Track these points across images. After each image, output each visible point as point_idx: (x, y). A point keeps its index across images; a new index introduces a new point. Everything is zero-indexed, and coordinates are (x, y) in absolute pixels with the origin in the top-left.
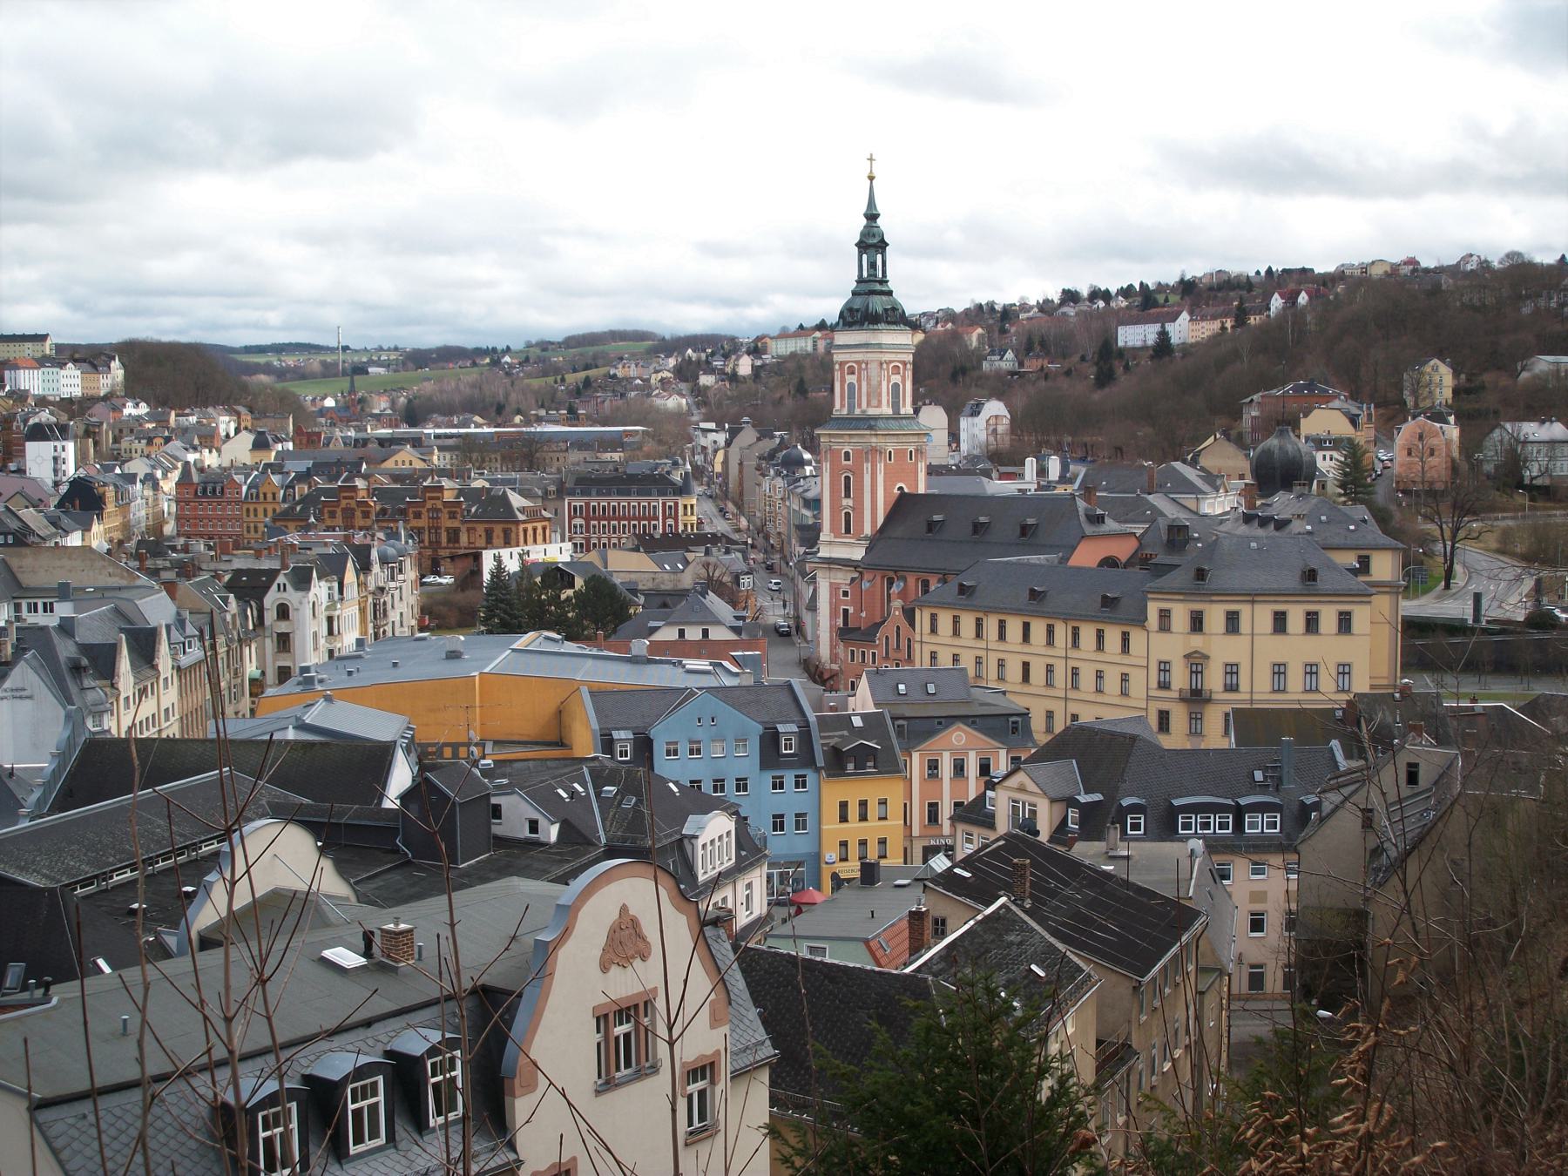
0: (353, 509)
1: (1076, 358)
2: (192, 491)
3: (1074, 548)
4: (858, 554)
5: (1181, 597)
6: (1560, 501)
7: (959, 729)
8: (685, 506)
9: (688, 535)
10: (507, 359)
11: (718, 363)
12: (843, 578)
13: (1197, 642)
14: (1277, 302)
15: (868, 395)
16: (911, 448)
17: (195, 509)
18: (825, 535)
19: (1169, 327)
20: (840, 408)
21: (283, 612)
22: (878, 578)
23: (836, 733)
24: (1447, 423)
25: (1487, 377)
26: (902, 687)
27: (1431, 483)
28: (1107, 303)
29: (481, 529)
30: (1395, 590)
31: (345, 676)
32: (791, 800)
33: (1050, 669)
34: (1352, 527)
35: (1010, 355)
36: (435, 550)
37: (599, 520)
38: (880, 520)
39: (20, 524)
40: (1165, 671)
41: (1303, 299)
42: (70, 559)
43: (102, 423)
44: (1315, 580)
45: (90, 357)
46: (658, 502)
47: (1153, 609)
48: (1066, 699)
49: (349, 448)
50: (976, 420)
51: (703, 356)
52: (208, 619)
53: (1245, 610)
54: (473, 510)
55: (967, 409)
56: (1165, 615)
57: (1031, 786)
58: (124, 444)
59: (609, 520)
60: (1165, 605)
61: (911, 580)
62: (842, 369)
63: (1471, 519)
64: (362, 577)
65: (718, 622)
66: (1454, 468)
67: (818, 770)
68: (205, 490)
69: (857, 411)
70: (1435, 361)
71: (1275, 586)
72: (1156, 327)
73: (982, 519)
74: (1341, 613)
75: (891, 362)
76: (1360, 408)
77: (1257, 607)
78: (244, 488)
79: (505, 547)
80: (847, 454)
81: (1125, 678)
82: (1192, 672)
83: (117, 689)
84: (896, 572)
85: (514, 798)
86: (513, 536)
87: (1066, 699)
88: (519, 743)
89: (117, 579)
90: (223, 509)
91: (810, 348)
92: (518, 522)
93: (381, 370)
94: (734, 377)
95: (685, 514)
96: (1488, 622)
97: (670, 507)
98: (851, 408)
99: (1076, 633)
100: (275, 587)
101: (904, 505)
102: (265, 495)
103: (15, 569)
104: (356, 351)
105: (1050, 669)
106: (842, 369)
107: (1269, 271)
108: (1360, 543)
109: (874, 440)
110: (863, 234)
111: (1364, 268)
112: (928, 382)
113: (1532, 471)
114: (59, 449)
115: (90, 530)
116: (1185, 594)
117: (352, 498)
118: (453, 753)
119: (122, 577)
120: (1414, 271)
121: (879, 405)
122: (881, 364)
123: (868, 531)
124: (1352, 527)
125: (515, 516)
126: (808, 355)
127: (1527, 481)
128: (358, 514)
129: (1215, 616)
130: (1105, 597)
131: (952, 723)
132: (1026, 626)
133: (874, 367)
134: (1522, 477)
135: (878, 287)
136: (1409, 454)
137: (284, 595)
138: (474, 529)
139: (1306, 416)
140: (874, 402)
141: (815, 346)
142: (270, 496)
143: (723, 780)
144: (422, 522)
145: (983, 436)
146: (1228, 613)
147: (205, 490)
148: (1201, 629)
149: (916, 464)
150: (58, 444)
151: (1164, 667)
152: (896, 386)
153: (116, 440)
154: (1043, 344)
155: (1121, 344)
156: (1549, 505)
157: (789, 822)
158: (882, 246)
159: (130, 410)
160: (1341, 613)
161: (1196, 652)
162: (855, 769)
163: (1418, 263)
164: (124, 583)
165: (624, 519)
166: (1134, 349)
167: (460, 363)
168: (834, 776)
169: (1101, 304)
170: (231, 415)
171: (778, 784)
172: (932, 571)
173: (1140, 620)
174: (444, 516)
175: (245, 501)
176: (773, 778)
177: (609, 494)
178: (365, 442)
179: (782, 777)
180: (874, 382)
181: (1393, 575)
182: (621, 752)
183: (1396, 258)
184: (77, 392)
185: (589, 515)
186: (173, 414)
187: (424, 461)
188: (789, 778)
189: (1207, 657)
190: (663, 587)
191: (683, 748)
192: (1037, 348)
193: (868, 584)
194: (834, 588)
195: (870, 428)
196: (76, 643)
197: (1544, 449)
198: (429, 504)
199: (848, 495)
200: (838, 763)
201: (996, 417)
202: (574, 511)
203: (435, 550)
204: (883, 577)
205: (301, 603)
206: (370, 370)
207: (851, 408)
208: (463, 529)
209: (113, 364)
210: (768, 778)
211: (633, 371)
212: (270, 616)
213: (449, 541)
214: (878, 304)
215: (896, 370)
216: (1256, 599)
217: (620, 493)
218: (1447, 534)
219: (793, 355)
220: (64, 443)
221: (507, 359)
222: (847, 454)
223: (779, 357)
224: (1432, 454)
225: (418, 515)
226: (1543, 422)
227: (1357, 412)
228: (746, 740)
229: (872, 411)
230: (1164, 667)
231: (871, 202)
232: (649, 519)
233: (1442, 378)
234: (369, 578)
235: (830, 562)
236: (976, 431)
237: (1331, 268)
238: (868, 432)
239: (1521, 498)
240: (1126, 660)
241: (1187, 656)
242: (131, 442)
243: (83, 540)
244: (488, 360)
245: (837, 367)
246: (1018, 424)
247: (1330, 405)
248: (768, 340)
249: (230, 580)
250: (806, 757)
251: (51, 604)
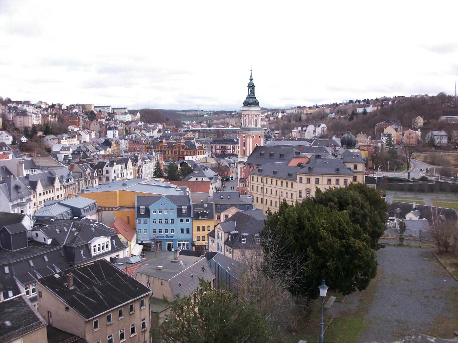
0: (180, 147)
2: (133, 142)
3: (291, 161)
4: (245, 160)
5: (305, 174)
6: (442, 149)
7: (233, 208)
8: (237, 147)
9: (227, 154)
10: (233, 113)
11: (274, 115)
12: (242, 166)
13: (308, 186)
15: (249, 122)
16: (260, 135)
17: (133, 146)
19: (366, 108)
21: (107, 172)
22: (248, 166)
23: (199, 208)
24: (418, 131)
25: (431, 121)
26: (222, 196)
27: (412, 145)
28: (359, 103)
29: (189, 151)
30: (363, 174)
31: (96, 189)
32: (185, 225)
33: (276, 191)
34: (353, 157)
36: (179, 156)
37: (218, 150)
38: (251, 152)
39: (86, 149)
40: (301, 193)
42: (46, 160)
43: (131, 127)
44: (338, 171)
45: (133, 112)
47: (298, 177)
48: (280, 199)
49: (184, 132)
50: (319, 128)
51: (272, 113)
52: (80, 174)
53: (320, 178)
54: (187, 147)
55: (317, 126)
56: (301, 179)
58: (136, 131)
59: (220, 150)
60: (301, 176)
61: (255, 167)
62: (243, 116)
63: (414, 153)
64: (134, 163)
65: (205, 177)
66: (418, 142)
67: (192, 218)
68: (135, 142)
69: (246, 126)
70: (419, 117)
71: (328, 172)
72: (363, 108)
73: (272, 153)
74: (345, 180)
75: (255, 114)
76: (398, 127)
77: (323, 177)
78: (143, 141)
79: (190, 156)
81: (292, 194)
82: (307, 193)
83: (36, 192)
84: (251, 165)
85: (40, 232)
86: (196, 153)
87: (280, 199)
88: (128, 207)
89: (56, 164)
91: (294, 112)
92: (197, 150)
93: (207, 116)
94: (277, 118)
95: (237, 149)
96: (411, 179)
97: (234, 147)
100: (105, 166)
101: (257, 149)
102: (148, 143)
103: (35, 162)
104: (205, 111)
105: (276, 191)
106: (243, 116)
107: (395, 97)
108: (355, 161)
109: (249, 133)
110: (249, 84)
111: (416, 96)
112: (316, 120)
113: (436, 142)
114: (115, 132)
115: (106, 150)
116: (306, 174)
117: (162, 144)
118: (112, 209)
119: (57, 164)
121: (251, 124)
122: (252, 115)
123: (248, 155)
124: (353, 157)
125: (196, 148)
126: (294, 113)
127: (435, 145)
128: (163, 147)
129: (313, 179)
130: (288, 174)
131: (232, 207)
132: (272, 180)
133: (250, 116)
134: (434, 144)
135: (252, 96)
136: (407, 138)
137: (107, 168)
138: (187, 151)
139: (385, 129)
140: (250, 124)
141: (295, 111)
142: (148, 143)
143: (167, 220)
144: (177, 150)
145: (320, 132)
146: (316, 179)
147: (135, 142)
148: (309, 183)
149: (261, 139)
150: (114, 131)
151: (301, 192)
152: (256, 120)
153: (135, 130)
155: (357, 112)
156: (439, 150)
157: (185, 231)
158: (253, 86)
159: (140, 124)
160: (345, 180)
161: (308, 188)
162: (202, 218)
163: (428, 95)
164: (58, 165)
165: (221, 149)
166: (360, 113)
167: (224, 114)
168: (195, 219)
169: (358, 103)
170: (162, 125)
171: (182, 221)
173: (295, 180)
174: (181, 148)
175: (144, 144)
176: (187, 219)
177: (220, 144)
179: (183, 219)
180: (250, 119)
181: (362, 169)
182: (142, 212)
183: (423, 94)
184: (130, 120)
185: (216, 148)
186: (148, 125)
187: (194, 135)
188: (185, 220)
189: (311, 190)
190: (213, 166)
191: (157, 211)
192: (340, 113)
193: (246, 168)
194: (241, 168)
195: (249, 130)
196: (29, 180)
197: (439, 137)
198: (178, 146)
199: (244, 146)
200: (197, 217)
201: (324, 127)
202: (213, 148)
203: (179, 156)
204: (249, 166)
205: (111, 170)
206: (204, 115)
208: (185, 151)
209: (138, 114)
210: (179, 219)
212: (104, 173)
213: (182, 154)
214: (251, 100)
215: (256, 116)
216: (323, 175)
217: (222, 144)
218: (408, 157)
219: (291, 113)
220: (116, 131)
221: (233, 113)
222: (244, 136)
223: (288, 114)
224: (412, 138)
225: (176, 148)
226: (440, 131)
227: (397, 128)
228: (173, 210)
229: (250, 126)
230: (301, 192)
232: (229, 150)
233: (420, 121)
234: (137, 164)
235: (240, 162)
236: (319, 131)
238: (248, 131)
239: (433, 149)
240: (292, 190)
241: (306, 189)
242: (137, 130)
243: (105, 152)
244: (229, 114)
245: (242, 115)
246: (328, 129)
247: (391, 126)
248: (286, 110)
249: (97, 164)
250: (189, 215)
251: (36, 170)
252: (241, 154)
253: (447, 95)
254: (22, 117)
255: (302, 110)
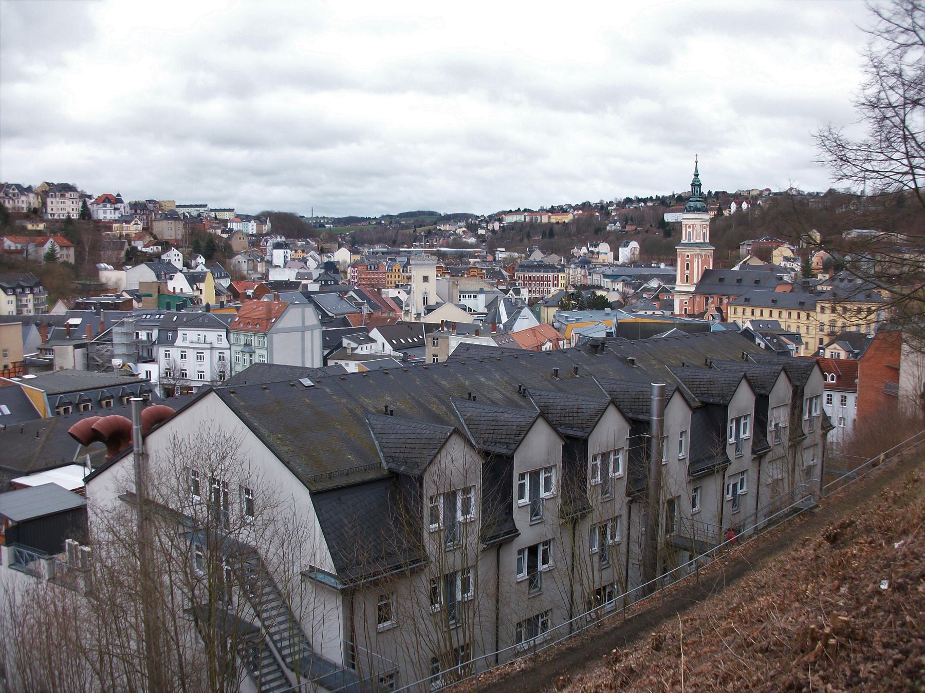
1: (648, 225)
4: (693, 289)
12: (686, 298)
14: (733, 206)
17: (366, 275)
18: (678, 282)
20: (684, 239)
35: (618, 224)
41: (745, 205)
46: (551, 275)
57: (839, 348)
80: (688, 256)
90: (378, 275)
94: (493, 230)
98: (689, 240)
99: (790, 314)
111: (749, 192)
120: (770, 194)
123: (695, 281)
142: (397, 271)
154: (632, 220)
169: (643, 204)
172: (724, 295)
173: (814, 310)
178: (377, 253)
184: (255, 232)
194: (681, 301)
199: (687, 269)
207: (689, 240)
211: (448, 227)
215: (690, 227)
219: (516, 222)
222: (688, 256)
231: (696, 170)
237: (734, 192)
252: (682, 281)
253: (806, 193)
254: (173, 222)
255: (539, 217)
